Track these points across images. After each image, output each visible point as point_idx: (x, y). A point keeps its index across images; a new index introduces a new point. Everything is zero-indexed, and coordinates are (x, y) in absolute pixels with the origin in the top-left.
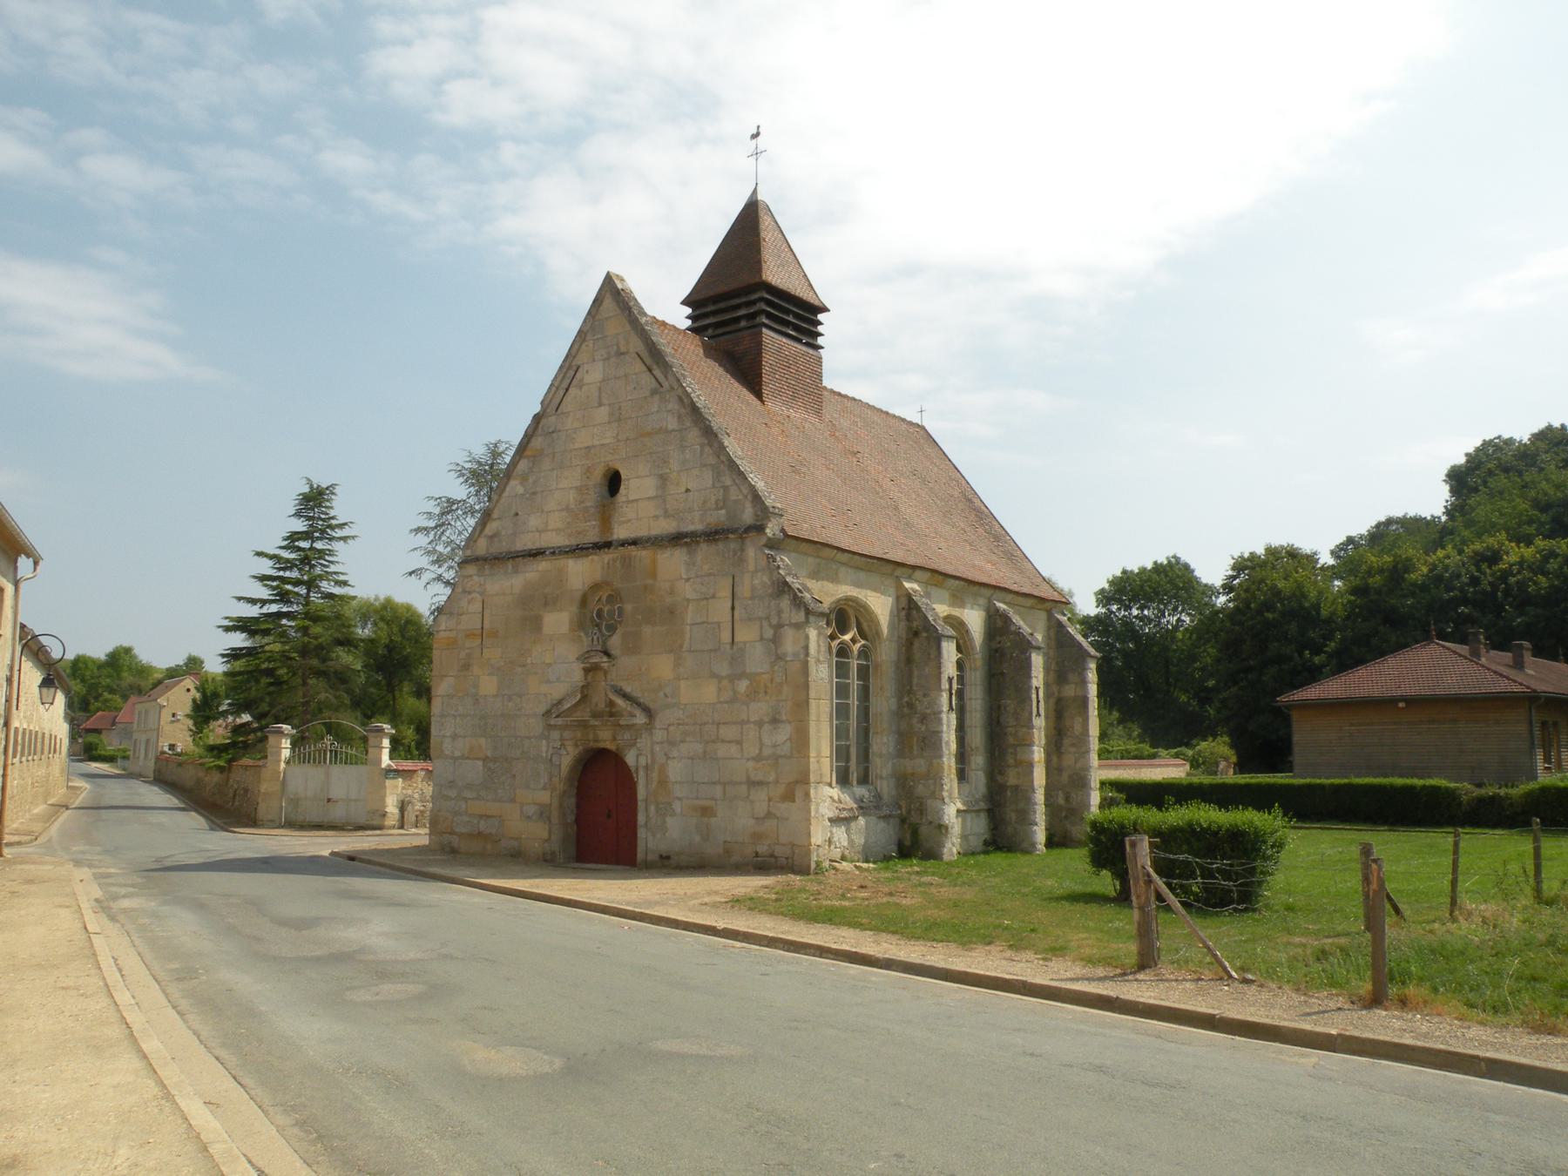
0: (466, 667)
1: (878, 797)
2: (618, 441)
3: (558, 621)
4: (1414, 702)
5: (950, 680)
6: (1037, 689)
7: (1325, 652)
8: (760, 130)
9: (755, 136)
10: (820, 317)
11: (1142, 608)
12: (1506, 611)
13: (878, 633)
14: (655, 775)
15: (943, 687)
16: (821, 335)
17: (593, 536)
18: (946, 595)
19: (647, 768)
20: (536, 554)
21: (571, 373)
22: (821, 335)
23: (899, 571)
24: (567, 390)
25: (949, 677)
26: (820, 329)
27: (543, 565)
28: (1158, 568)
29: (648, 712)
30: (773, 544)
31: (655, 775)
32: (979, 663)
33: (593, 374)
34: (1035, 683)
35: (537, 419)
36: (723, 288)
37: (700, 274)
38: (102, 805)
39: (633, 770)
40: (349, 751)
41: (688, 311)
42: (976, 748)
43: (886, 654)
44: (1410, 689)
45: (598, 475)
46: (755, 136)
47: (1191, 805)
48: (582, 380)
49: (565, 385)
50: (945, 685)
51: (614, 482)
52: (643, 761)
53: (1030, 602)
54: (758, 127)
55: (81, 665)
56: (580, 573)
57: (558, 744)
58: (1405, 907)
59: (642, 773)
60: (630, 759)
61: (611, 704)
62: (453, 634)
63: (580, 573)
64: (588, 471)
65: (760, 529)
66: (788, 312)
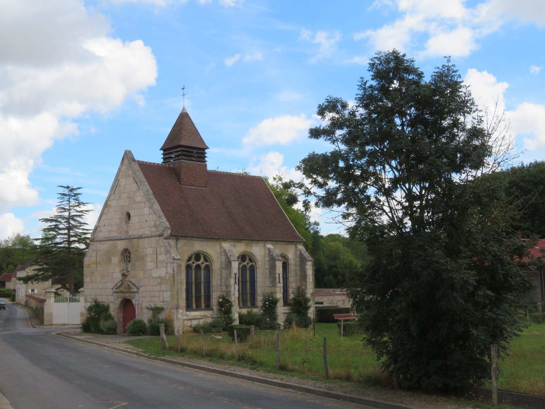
0: (93, 273)
2: (130, 204)
3: (116, 259)
5: (235, 274)
6: (279, 274)
8: (185, 87)
9: (183, 89)
10: (206, 151)
11: (439, 217)
14: (140, 307)
15: (232, 277)
16: (207, 157)
19: (138, 304)
21: (117, 182)
22: (207, 157)
24: (116, 187)
25: (235, 274)
26: (206, 155)
29: (138, 288)
31: (140, 307)
33: (123, 182)
34: (278, 272)
36: (170, 146)
37: (166, 139)
39: (134, 305)
40: (74, 297)
41: (162, 152)
42: (259, 294)
45: (125, 215)
46: (183, 89)
48: (120, 184)
49: (116, 185)
50: (233, 276)
51: (129, 216)
52: (137, 303)
54: (184, 86)
56: (121, 245)
57: (116, 298)
58: (275, 337)
59: (137, 306)
60: (134, 302)
61: (129, 285)
62: (89, 263)
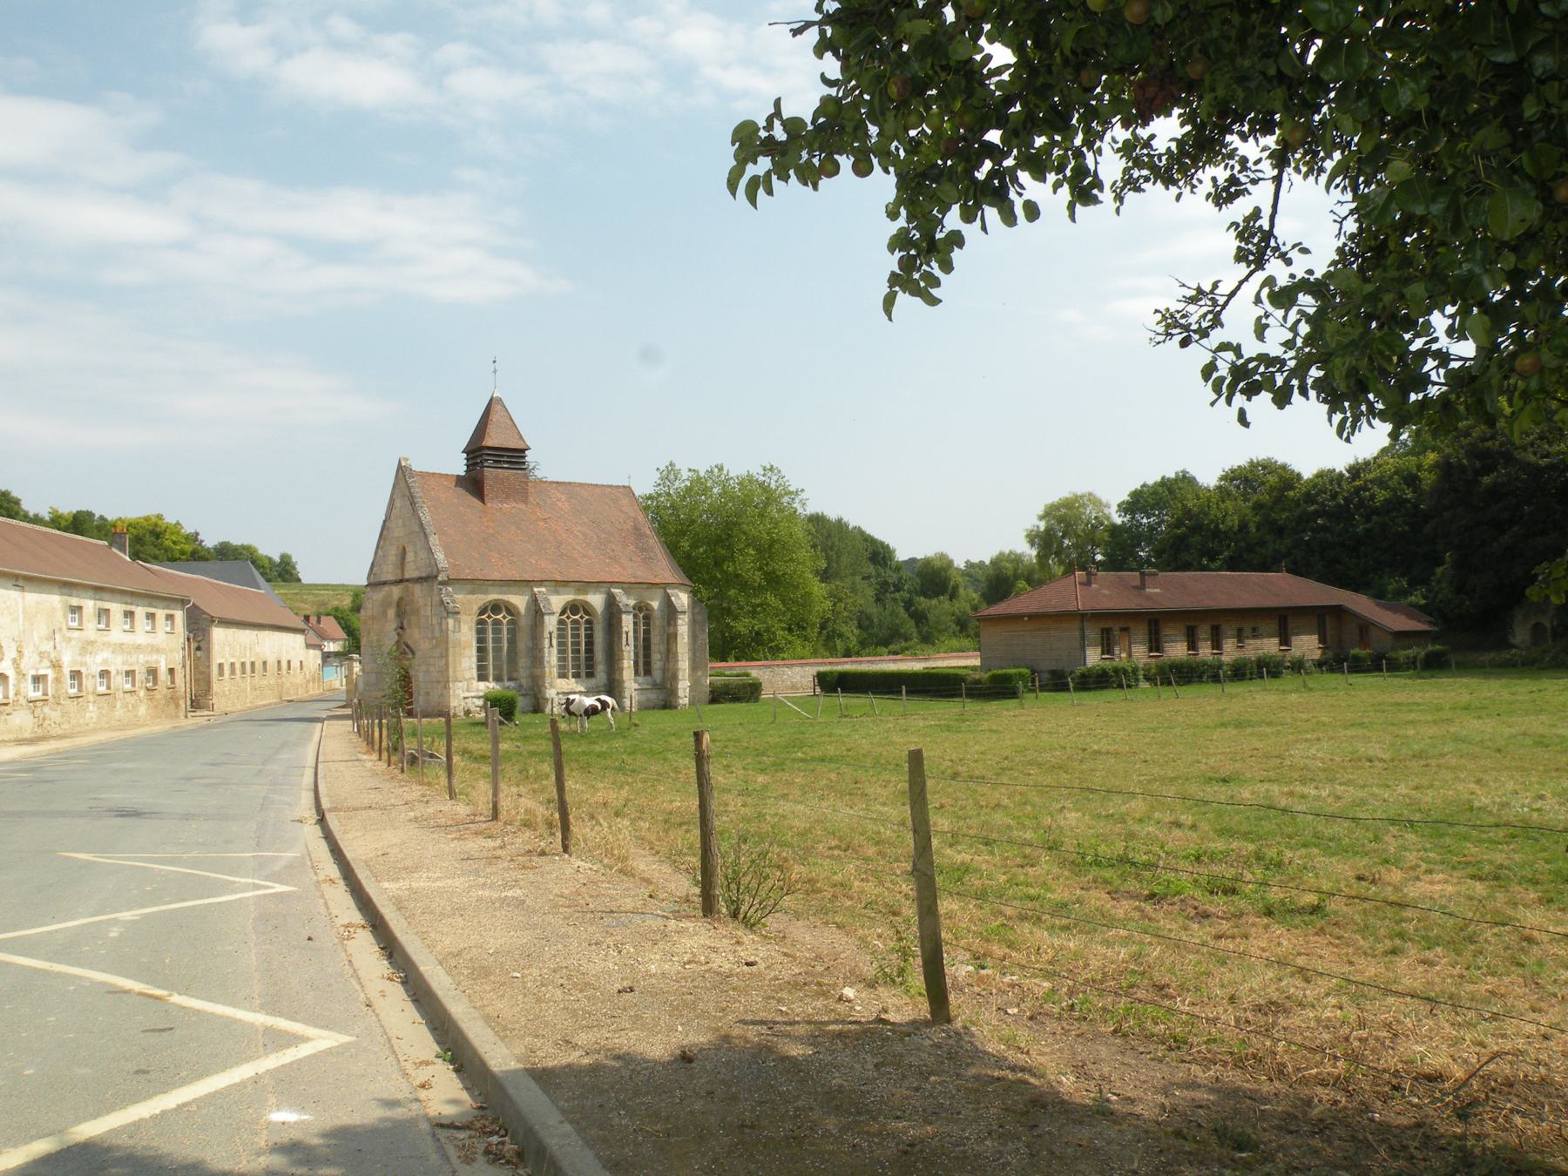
1: (521, 686)
4: (1034, 617)
6: (627, 633)
7: (1220, 559)
12: (1355, 519)
13: (519, 613)
17: (400, 577)
18: (573, 590)
20: (385, 583)
23: (532, 584)
27: (386, 588)
28: (1165, 483)
30: (443, 583)
32: (601, 620)
33: (398, 504)
35: (385, 521)
38: (313, 780)
43: (524, 622)
44: (1033, 609)
47: (399, 672)
53: (645, 586)
55: (1304, 169)
63: (396, 591)
64: (398, 547)
65: (436, 577)
66: (503, 456)
